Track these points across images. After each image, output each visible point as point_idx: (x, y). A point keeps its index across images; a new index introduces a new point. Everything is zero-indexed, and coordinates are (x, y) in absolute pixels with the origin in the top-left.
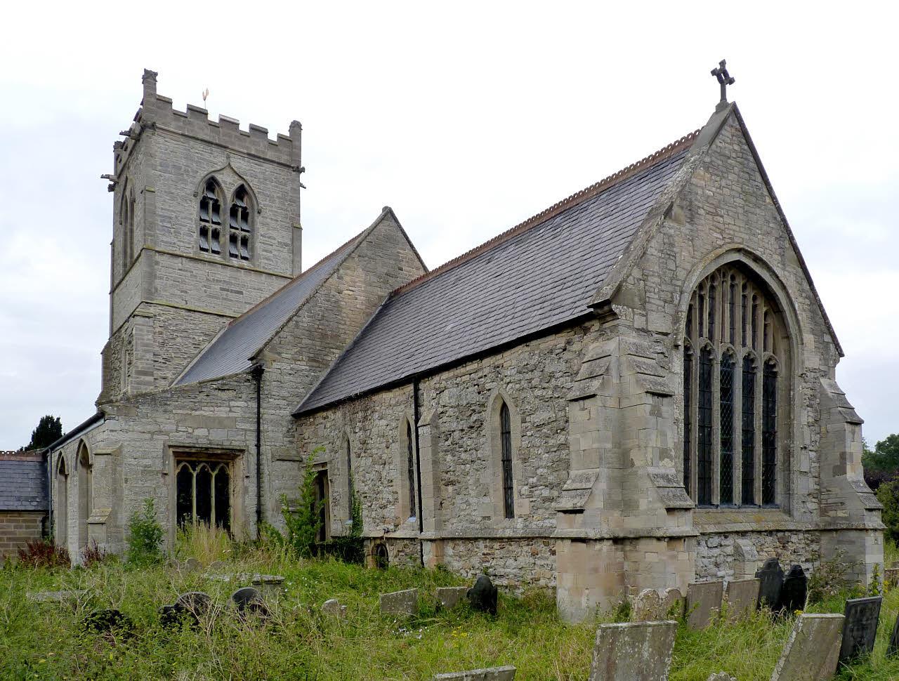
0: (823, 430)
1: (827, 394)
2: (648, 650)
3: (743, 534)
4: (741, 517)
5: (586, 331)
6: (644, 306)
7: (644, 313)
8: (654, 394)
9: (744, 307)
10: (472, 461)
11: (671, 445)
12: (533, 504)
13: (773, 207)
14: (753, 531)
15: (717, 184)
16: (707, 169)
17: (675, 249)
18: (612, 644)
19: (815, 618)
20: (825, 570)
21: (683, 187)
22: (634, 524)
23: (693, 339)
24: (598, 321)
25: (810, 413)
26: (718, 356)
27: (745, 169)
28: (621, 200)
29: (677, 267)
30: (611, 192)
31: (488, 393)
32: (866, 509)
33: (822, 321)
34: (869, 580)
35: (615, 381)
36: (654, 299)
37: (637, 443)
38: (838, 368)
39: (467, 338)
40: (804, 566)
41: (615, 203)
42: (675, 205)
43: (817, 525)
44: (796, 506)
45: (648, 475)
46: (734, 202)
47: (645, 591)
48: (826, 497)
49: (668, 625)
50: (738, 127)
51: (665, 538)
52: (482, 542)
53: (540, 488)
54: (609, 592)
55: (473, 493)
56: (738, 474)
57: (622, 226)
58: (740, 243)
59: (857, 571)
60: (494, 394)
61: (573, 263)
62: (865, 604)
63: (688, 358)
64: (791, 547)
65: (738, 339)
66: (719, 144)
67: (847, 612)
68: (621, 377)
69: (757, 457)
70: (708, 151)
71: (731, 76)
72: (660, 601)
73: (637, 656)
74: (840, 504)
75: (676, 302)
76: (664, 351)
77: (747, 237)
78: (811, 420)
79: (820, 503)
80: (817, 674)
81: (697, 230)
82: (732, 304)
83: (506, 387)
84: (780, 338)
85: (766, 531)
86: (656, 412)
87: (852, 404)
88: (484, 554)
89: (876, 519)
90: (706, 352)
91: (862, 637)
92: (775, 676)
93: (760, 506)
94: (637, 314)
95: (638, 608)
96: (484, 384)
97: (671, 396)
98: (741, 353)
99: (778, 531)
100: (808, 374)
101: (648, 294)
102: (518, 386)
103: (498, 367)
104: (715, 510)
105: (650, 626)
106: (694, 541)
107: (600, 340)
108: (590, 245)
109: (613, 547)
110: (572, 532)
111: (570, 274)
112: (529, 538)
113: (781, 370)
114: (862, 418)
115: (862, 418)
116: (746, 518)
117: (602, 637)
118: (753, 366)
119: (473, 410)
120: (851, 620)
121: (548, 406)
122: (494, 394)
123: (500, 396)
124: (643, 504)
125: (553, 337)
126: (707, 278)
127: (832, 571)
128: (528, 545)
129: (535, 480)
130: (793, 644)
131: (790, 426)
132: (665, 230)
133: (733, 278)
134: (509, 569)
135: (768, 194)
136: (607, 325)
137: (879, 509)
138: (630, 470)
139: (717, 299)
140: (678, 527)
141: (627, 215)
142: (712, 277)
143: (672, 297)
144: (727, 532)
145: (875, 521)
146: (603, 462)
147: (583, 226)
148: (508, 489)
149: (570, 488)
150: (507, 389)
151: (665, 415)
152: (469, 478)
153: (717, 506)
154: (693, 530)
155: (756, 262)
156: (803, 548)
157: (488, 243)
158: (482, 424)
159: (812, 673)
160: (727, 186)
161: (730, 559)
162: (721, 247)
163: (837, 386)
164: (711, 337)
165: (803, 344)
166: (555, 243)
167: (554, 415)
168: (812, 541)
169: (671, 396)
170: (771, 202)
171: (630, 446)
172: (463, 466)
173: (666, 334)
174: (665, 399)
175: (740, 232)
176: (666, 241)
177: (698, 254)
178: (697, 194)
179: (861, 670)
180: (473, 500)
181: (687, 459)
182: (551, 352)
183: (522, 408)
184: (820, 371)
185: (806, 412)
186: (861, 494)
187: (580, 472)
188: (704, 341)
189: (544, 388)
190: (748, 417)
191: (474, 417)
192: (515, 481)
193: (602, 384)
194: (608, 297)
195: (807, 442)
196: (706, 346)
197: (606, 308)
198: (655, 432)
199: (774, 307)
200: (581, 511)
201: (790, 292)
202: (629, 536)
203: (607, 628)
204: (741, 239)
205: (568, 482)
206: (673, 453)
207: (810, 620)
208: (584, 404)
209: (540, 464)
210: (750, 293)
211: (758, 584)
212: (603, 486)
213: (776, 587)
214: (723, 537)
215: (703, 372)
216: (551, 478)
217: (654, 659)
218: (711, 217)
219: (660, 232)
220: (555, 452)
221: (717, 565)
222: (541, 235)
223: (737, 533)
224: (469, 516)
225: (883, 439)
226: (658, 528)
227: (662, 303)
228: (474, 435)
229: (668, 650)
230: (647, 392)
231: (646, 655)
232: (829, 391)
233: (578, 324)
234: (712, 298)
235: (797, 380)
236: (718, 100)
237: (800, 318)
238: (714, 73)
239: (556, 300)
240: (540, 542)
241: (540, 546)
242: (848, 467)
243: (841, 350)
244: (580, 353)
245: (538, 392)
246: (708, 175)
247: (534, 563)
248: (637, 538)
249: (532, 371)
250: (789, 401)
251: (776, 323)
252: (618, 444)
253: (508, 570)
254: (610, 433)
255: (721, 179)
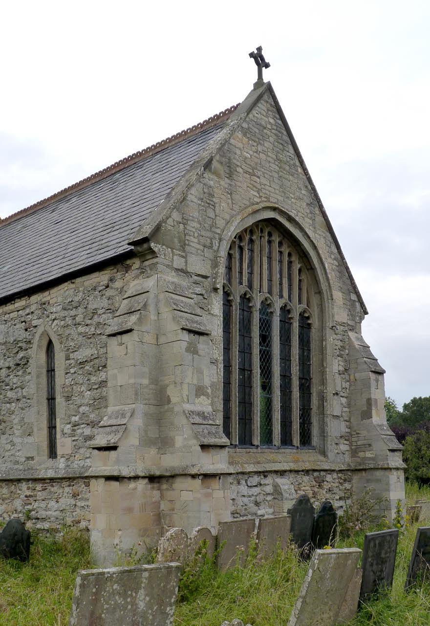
0: (352, 377)
1: (354, 346)
2: (144, 599)
3: (282, 473)
4: (279, 457)
5: (128, 268)
6: (184, 248)
7: (183, 254)
8: (190, 331)
9: (281, 262)
10: (17, 400)
11: (207, 382)
12: (75, 443)
13: (304, 177)
14: (291, 471)
15: (254, 149)
16: (245, 135)
17: (214, 200)
18: (96, 594)
19: (331, 554)
20: (355, 507)
21: (223, 145)
22: (170, 462)
23: (233, 286)
24: (138, 259)
25: (340, 363)
26: (257, 303)
27: (279, 140)
28: (172, 159)
29: (216, 216)
30: (164, 153)
31: (35, 330)
32: (389, 450)
33: (348, 282)
34: (394, 516)
35: (153, 317)
36: (194, 243)
37: (174, 379)
38: (364, 323)
39: (20, 277)
40: (336, 504)
41: (166, 161)
42: (214, 160)
43: (349, 465)
44: (329, 447)
45: (184, 411)
46: (270, 166)
47: (172, 531)
48: (356, 439)
49: (170, 567)
50: (273, 103)
51: (199, 475)
52: (24, 483)
53: (82, 426)
54: (144, 533)
55: (17, 433)
56: (277, 416)
57: (169, 179)
58: (275, 203)
59: (383, 507)
60: (40, 330)
61: (123, 210)
62: (383, 536)
63: (227, 304)
64: (326, 486)
65: (276, 290)
66: (256, 115)
67: (366, 549)
68: (159, 313)
69: (295, 401)
70: (245, 118)
71: (267, 61)
72: (189, 541)
73: (129, 607)
74: (367, 446)
75: (215, 248)
76: (204, 292)
77: (281, 199)
78: (341, 368)
79: (351, 445)
80: (337, 615)
81: (236, 185)
82: (270, 258)
83: (52, 324)
84: (313, 293)
85: (303, 471)
86: (192, 349)
87: (376, 356)
88: (26, 496)
89: (397, 458)
90: (246, 299)
91: (382, 571)
92: (293, 620)
93: (298, 447)
94: (176, 255)
95: (164, 549)
96: (31, 321)
97: (207, 334)
98: (278, 304)
99: (314, 471)
100: (338, 327)
101: (187, 237)
102: (62, 323)
103: (44, 304)
104: (255, 450)
105: (146, 570)
106: (230, 479)
107: (140, 277)
108: (140, 195)
109: (149, 486)
110: (105, 470)
111: (119, 219)
112: (70, 478)
113: (315, 321)
114: (384, 369)
115: (384, 367)
116: (284, 458)
117: (82, 586)
118: (290, 316)
119: (19, 347)
120: (370, 554)
121: (91, 343)
122: (40, 330)
123: (45, 333)
124: (179, 441)
125: (96, 274)
126: (245, 230)
127: (362, 507)
128: (69, 486)
129: (77, 418)
130: (309, 583)
131: (323, 373)
132: (206, 181)
133: (270, 235)
134: (50, 511)
135: (300, 165)
136: (147, 263)
137: (400, 450)
138: (166, 407)
139: (256, 251)
140: (213, 464)
141: (174, 170)
142: (251, 230)
143: (211, 243)
144: (267, 472)
145: (396, 461)
146: (139, 398)
147: (138, 180)
148: (52, 428)
149: (106, 424)
150: (53, 325)
151: (200, 352)
152: (14, 417)
153: (258, 446)
154: (228, 467)
155: (291, 222)
156: (337, 487)
157: (55, 196)
158: (28, 361)
159: (331, 614)
160: (264, 152)
161: (269, 498)
162: (257, 203)
163: (363, 340)
164: (250, 286)
165: (332, 299)
166: (111, 195)
167: (96, 352)
168: (345, 480)
169: (207, 334)
170: (303, 173)
171: (167, 382)
172: (8, 405)
173: (206, 277)
174: (201, 337)
175: (276, 194)
176: (206, 190)
177: (236, 207)
178: (235, 154)
179: (380, 605)
180: (17, 440)
181: (227, 400)
182: (95, 289)
183: (66, 345)
184: (348, 325)
185: (337, 361)
186: (385, 436)
187: (117, 408)
188: (243, 288)
189: (87, 325)
190: (285, 363)
191: (21, 354)
192: (58, 420)
193: (139, 319)
194: (147, 235)
195: (339, 389)
196: (245, 294)
197: (145, 246)
198: (191, 369)
199: (304, 256)
200: (114, 448)
201: (320, 252)
202: (165, 474)
203: (88, 575)
204: (276, 200)
205: (105, 418)
206: (209, 391)
207: (326, 556)
208: (121, 339)
209: (83, 401)
210: (286, 250)
211: (289, 521)
212: (138, 422)
213: (309, 523)
214: (262, 477)
215: (239, 315)
216: (92, 416)
217: (152, 610)
218: (249, 176)
219: (200, 182)
220: (97, 389)
221: (257, 504)
222: (101, 188)
223: (276, 472)
224: (12, 457)
225: (408, 401)
226: (193, 466)
227: (202, 248)
228: (20, 373)
229: (171, 598)
230: (183, 329)
231: (142, 605)
232: (356, 343)
233: (118, 261)
234: (252, 251)
235: (328, 332)
236: (255, 79)
237: (329, 276)
238: (252, 55)
239: (104, 241)
240: (81, 482)
241: (80, 487)
242: (374, 412)
243: (366, 309)
244: (121, 291)
245: (81, 329)
246: (245, 140)
247: (75, 505)
248: (173, 477)
249: (76, 307)
250: (322, 350)
251: (309, 278)
252: (155, 381)
253: (50, 513)
254: (146, 370)
255: (258, 145)
